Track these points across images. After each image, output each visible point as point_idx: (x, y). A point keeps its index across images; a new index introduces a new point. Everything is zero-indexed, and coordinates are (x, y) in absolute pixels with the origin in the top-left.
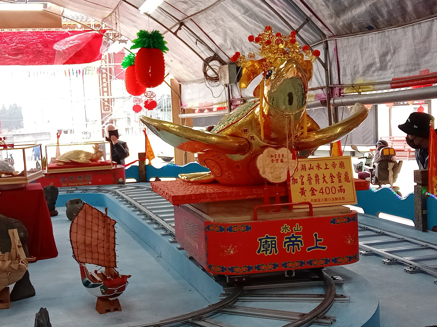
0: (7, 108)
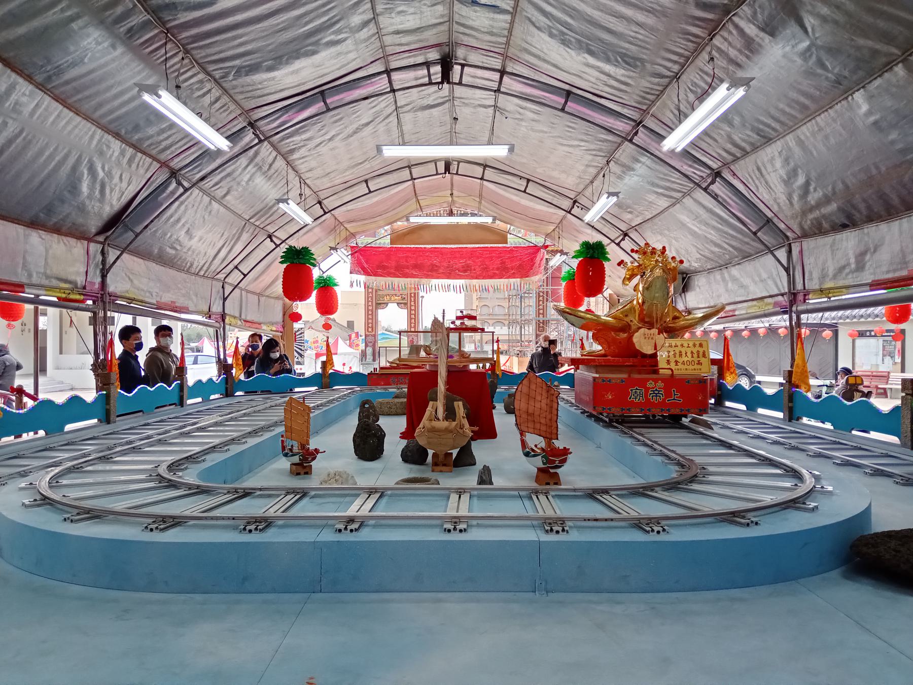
0: (851, 181)
